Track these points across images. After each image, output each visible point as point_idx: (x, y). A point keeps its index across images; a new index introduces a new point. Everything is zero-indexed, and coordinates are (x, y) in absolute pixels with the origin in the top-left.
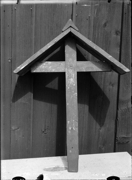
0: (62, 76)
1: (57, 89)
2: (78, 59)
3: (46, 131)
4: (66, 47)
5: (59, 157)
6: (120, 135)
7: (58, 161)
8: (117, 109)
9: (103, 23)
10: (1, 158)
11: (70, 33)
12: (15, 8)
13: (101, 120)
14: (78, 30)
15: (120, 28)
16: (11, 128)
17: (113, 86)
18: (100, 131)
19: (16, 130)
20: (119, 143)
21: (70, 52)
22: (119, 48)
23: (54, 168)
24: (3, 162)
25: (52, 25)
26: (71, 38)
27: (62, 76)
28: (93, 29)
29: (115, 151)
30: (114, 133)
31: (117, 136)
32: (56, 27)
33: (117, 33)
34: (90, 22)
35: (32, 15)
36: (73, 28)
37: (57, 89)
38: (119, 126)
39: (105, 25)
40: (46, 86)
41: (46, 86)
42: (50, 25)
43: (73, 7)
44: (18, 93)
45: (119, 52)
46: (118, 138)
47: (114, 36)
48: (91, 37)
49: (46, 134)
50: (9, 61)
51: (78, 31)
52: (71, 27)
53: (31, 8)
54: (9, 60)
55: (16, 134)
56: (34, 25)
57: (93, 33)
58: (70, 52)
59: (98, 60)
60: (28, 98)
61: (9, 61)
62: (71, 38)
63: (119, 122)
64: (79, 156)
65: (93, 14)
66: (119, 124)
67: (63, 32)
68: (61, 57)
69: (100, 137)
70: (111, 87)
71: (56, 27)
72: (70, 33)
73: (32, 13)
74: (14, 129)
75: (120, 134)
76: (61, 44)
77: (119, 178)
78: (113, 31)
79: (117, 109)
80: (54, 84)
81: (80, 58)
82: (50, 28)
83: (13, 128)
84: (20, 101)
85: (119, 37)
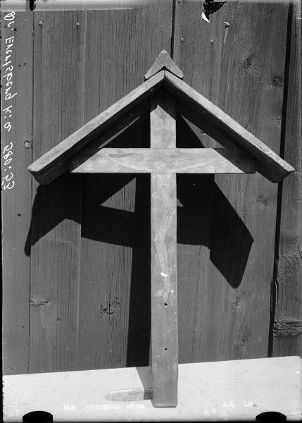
0: (143, 181)
1: (133, 210)
2: (180, 144)
3: (112, 307)
4: (152, 114)
5: (133, 370)
6: (282, 318)
7: (129, 378)
8: (276, 257)
9: (244, 58)
10: (3, 373)
11: (165, 81)
12: (41, 23)
13: (235, 280)
14: (181, 76)
15: (283, 69)
16: (30, 301)
17: (266, 204)
18: (236, 308)
19: (42, 306)
20: (280, 336)
21: (162, 124)
22: (280, 117)
23: (130, 394)
24: (6, 379)
25: (125, 64)
26: (165, 94)
27: (143, 181)
28: (219, 72)
29: (270, 355)
30: (269, 314)
31: (276, 320)
32: (134, 67)
33: (275, 82)
34: (213, 54)
35: (79, 38)
36: (170, 71)
37: (133, 210)
38: (280, 296)
39: (249, 62)
40: (105, 204)
41: (105, 204)
42: (120, 63)
43: (173, 24)
44: (42, 220)
45: (279, 126)
46: (278, 325)
47: (269, 87)
48: (216, 90)
49: (111, 315)
50: (27, 145)
51: (182, 79)
52: (164, 68)
53: (78, 24)
54: (27, 144)
55: (42, 314)
56: (84, 62)
57: (221, 80)
58: (162, 124)
59: (220, 146)
60: (67, 231)
61: (27, 145)
62: (165, 94)
63: (279, 287)
64: (184, 369)
65: (221, 37)
66: (280, 290)
67: (146, 80)
68: (140, 138)
69: (237, 323)
70: (262, 206)
71: (134, 67)
72: (165, 81)
73: (79, 34)
74: (36, 303)
75: (282, 315)
76: (141, 108)
77: (285, 417)
78: (267, 76)
79: (276, 257)
80: (122, 200)
81: (185, 139)
82: (120, 68)
83: (35, 301)
84: (49, 236)
85: (281, 90)
